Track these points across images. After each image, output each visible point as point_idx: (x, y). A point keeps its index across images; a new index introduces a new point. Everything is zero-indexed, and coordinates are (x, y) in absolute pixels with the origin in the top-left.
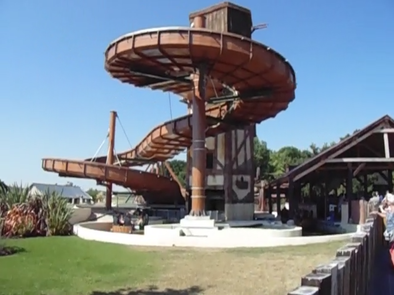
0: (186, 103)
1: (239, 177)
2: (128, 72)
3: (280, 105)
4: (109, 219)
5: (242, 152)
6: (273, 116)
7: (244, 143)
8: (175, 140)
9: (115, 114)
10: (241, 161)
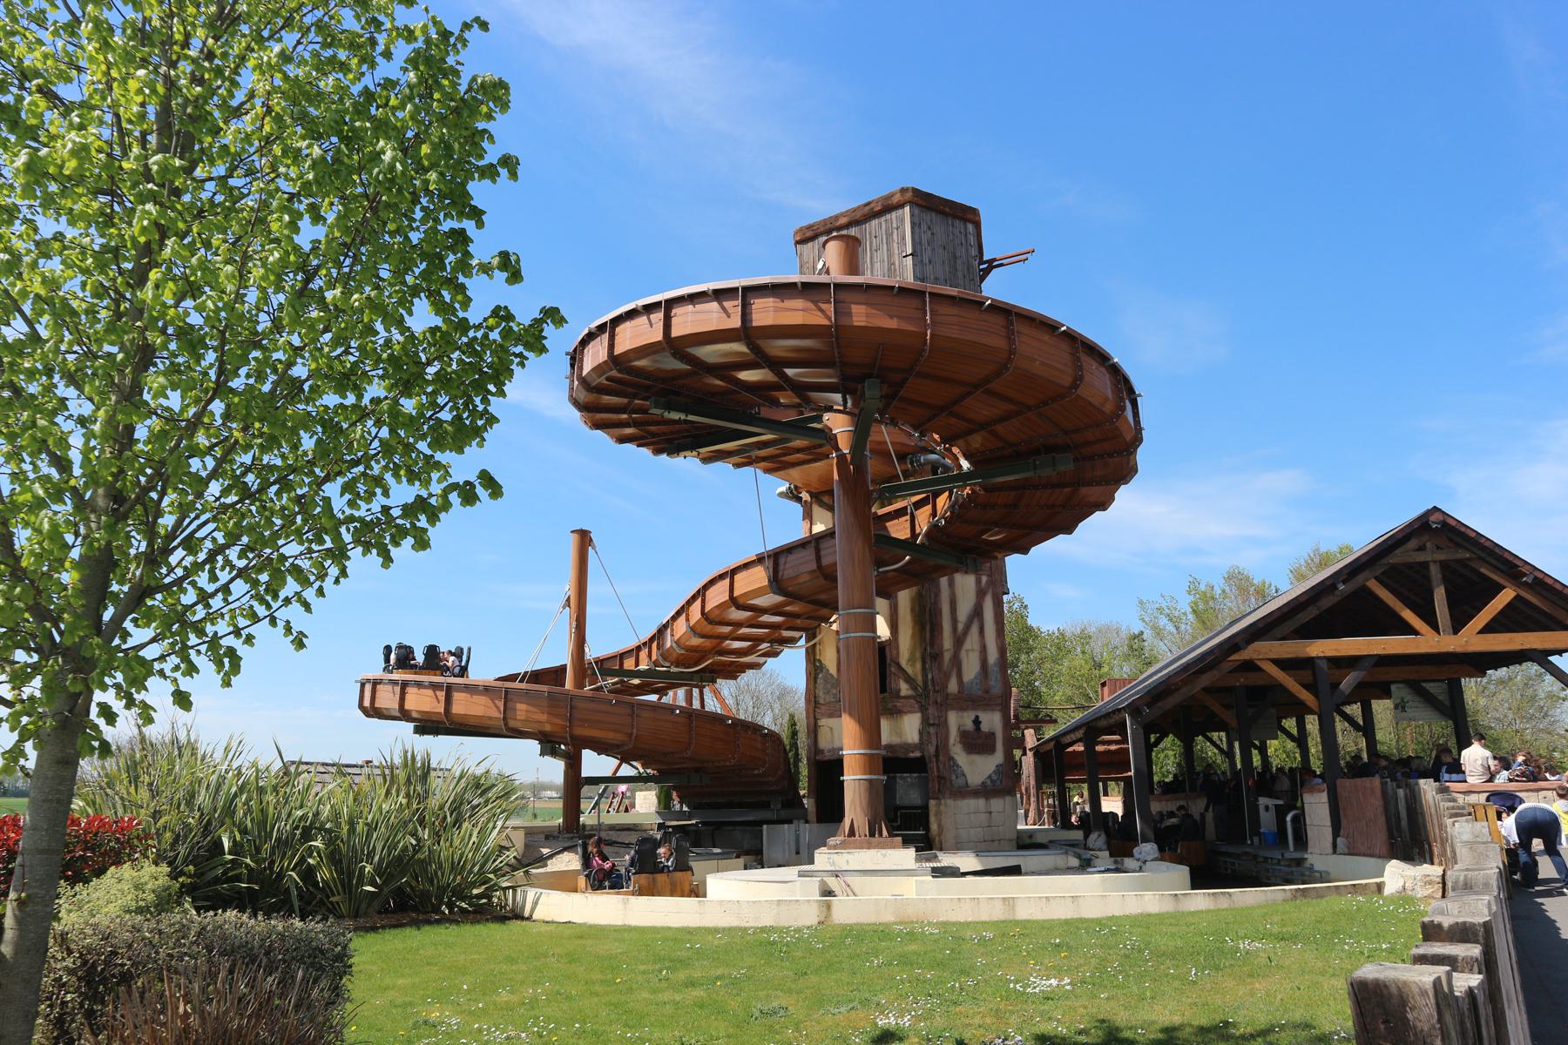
0: (799, 500)
1: (967, 719)
2: (645, 411)
3: (1092, 493)
4: (569, 862)
5: (972, 641)
6: (1068, 528)
7: (977, 613)
8: (775, 610)
9: (584, 538)
10: (971, 669)
